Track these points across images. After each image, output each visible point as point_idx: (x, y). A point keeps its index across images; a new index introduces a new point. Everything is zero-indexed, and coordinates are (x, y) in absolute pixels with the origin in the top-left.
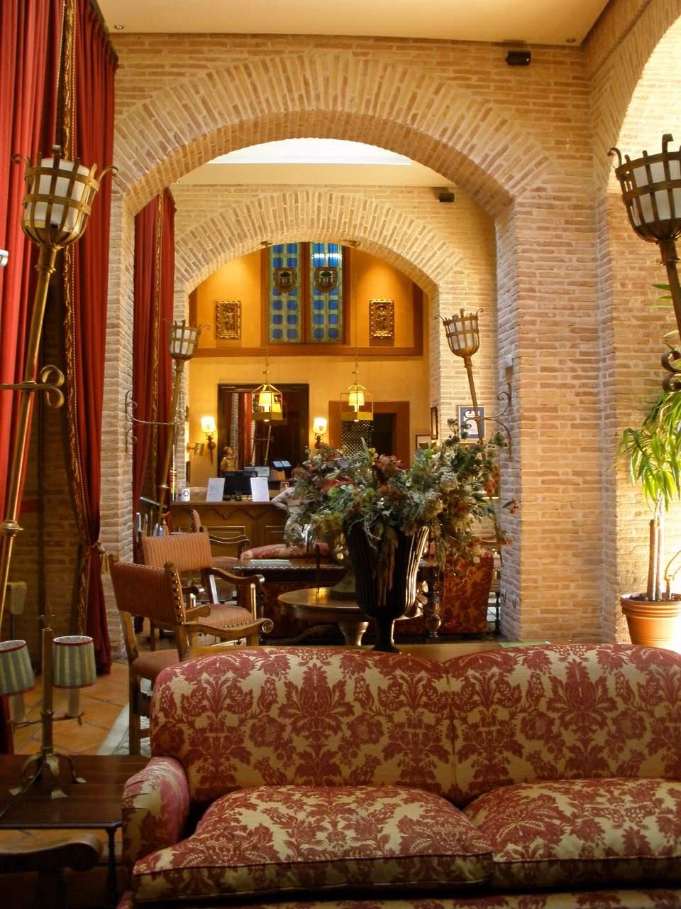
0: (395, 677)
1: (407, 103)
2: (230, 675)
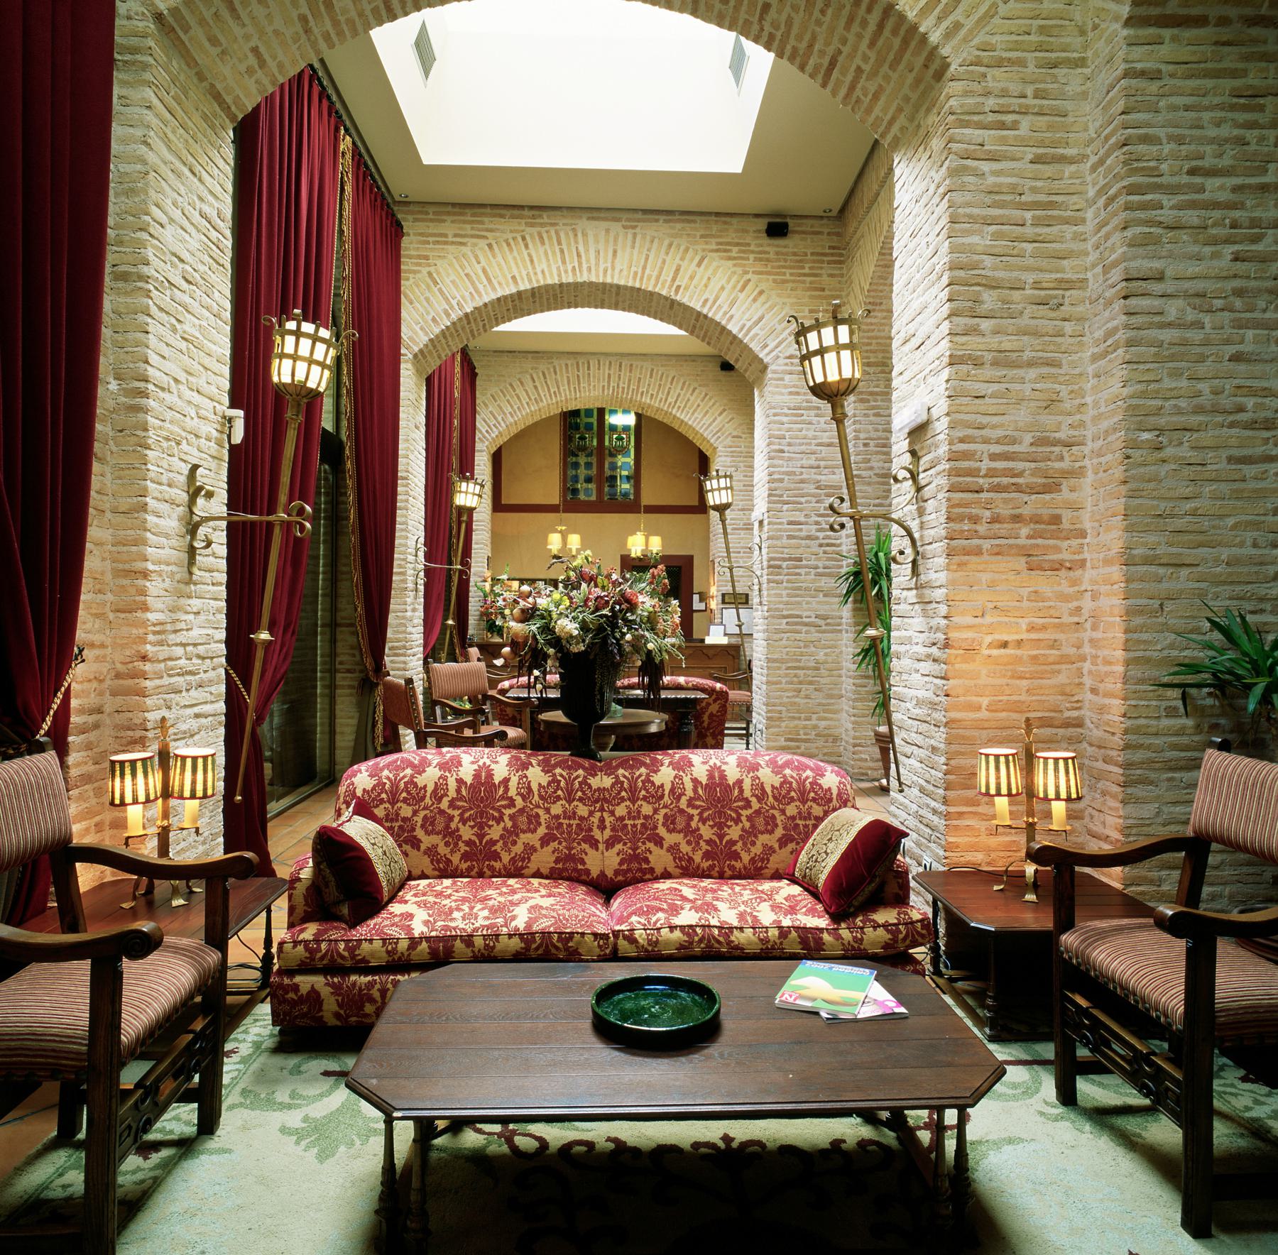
0: (554, 775)
1: (671, 275)
2: (409, 771)
